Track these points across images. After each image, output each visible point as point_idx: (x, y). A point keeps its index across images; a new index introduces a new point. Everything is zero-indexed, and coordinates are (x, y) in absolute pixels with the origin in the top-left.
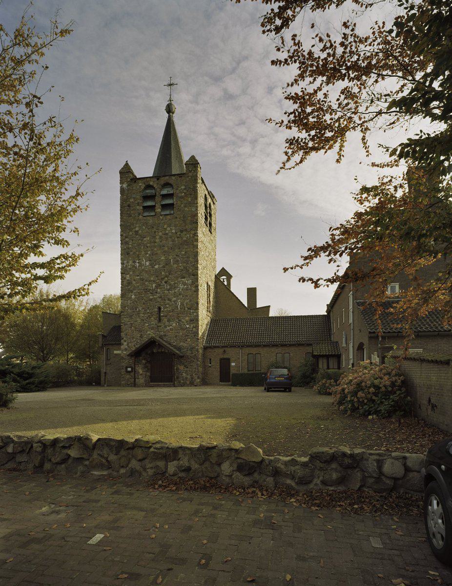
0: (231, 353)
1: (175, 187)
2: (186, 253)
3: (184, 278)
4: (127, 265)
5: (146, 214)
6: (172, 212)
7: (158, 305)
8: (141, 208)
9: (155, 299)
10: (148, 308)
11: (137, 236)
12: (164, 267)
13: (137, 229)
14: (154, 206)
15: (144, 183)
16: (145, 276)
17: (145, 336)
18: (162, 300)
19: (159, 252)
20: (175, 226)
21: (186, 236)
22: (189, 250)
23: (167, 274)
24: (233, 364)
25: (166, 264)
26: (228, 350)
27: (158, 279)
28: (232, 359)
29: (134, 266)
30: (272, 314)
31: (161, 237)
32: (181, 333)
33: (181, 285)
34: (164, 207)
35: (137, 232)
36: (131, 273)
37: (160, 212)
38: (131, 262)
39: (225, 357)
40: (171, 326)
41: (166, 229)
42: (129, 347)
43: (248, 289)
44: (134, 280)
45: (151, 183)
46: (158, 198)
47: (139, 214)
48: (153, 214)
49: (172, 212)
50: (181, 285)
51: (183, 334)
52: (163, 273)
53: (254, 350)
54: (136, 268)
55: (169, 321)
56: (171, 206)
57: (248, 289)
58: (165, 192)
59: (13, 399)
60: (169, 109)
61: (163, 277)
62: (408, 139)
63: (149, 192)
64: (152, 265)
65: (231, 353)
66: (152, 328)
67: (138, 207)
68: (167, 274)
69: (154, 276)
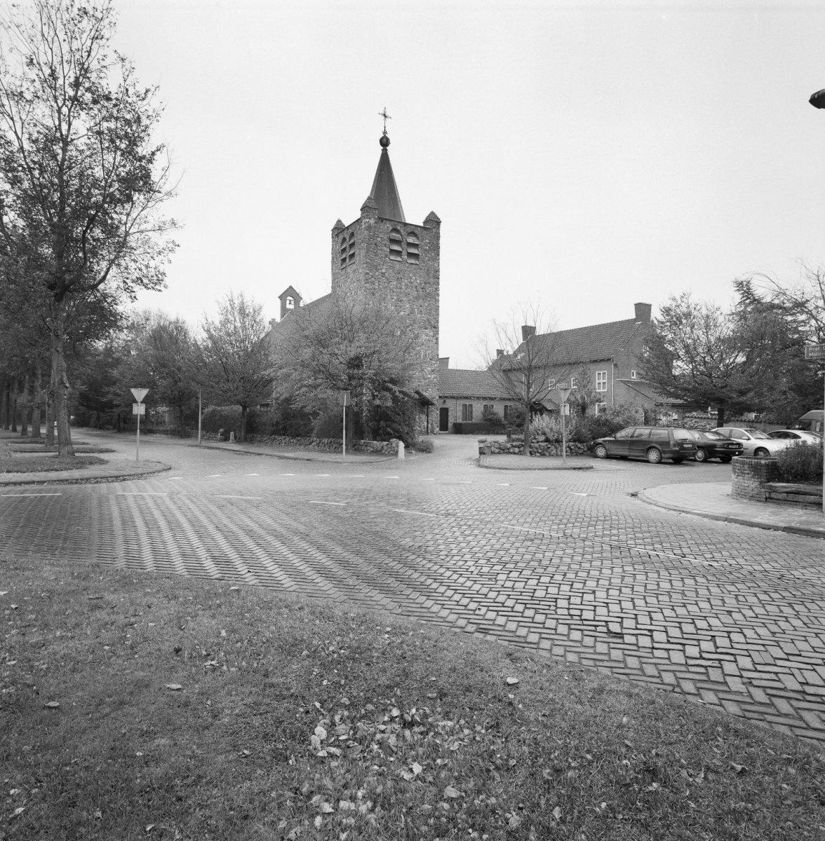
13: (384, 271)
14: (401, 252)
19: (404, 299)
20: (420, 277)
26: (448, 401)
30: (451, 366)
31: (406, 285)
34: (410, 255)
35: (384, 273)
41: (411, 278)
43: (291, 287)
45: (416, 232)
47: (386, 256)
53: (467, 402)
56: (415, 256)
57: (291, 287)
59: (156, 358)
60: (385, 142)
63: (395, 236)
65: (450, 404)
67: (385, 248)
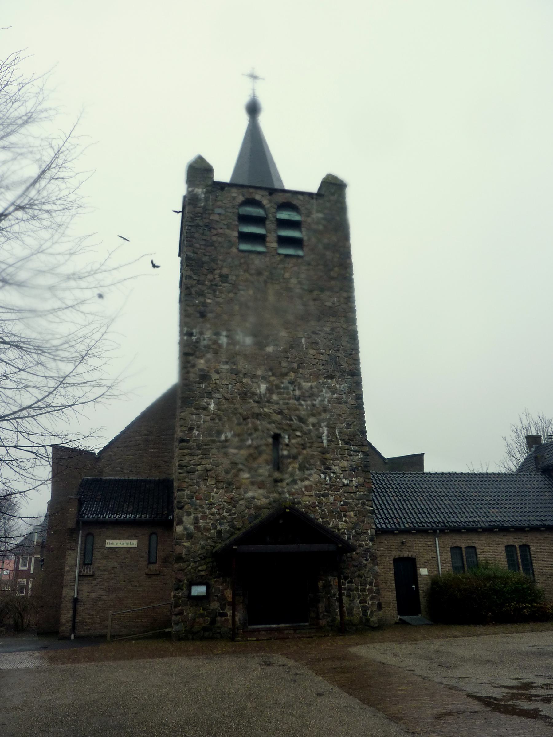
0: (416, 547)
1: (304, 212)
2: (332, 329)
3: (332, 378)
4: (199, 338)
5: (244, 247)
6: (300, 253)
7: (273, 429)
8: (236, 234)
9: (266, 415)
10: (250, 434)
11: (225, 285)
12: (286, 351)
15: (243, 195)
16: (244, 365)
17: (242, 502)
18: (285, 417)
21: (331, 300)
22: (337, 325)
23: (295, 366)
24: (424, 571)
25: (292, 347)
27: (273, 375)
28: (420, 560)
29: (215, 342)
30: (429, 467)
32: (331, 498)
33: (327, 393)
34: (284, 241)
36: (209, 356)
37: (276, 249)
38: (208, 334)
39: (406, 554)
40: (308, 479)
42: (198, 528)
44: (217, 372)
45: (258, 197)
46: (271, 225)
48: (261, 249)
49: (300, 253)
50: (327, 393)
51: (335, 500)
52: (284, 364)
54: (220, 346)
55: (302, 468)
58: (284, 215)
61: (284, 370)
62: (333, 188)
64: (260, 345)
66: (261, 485)
68: (295, 366)
69: (263, 367)
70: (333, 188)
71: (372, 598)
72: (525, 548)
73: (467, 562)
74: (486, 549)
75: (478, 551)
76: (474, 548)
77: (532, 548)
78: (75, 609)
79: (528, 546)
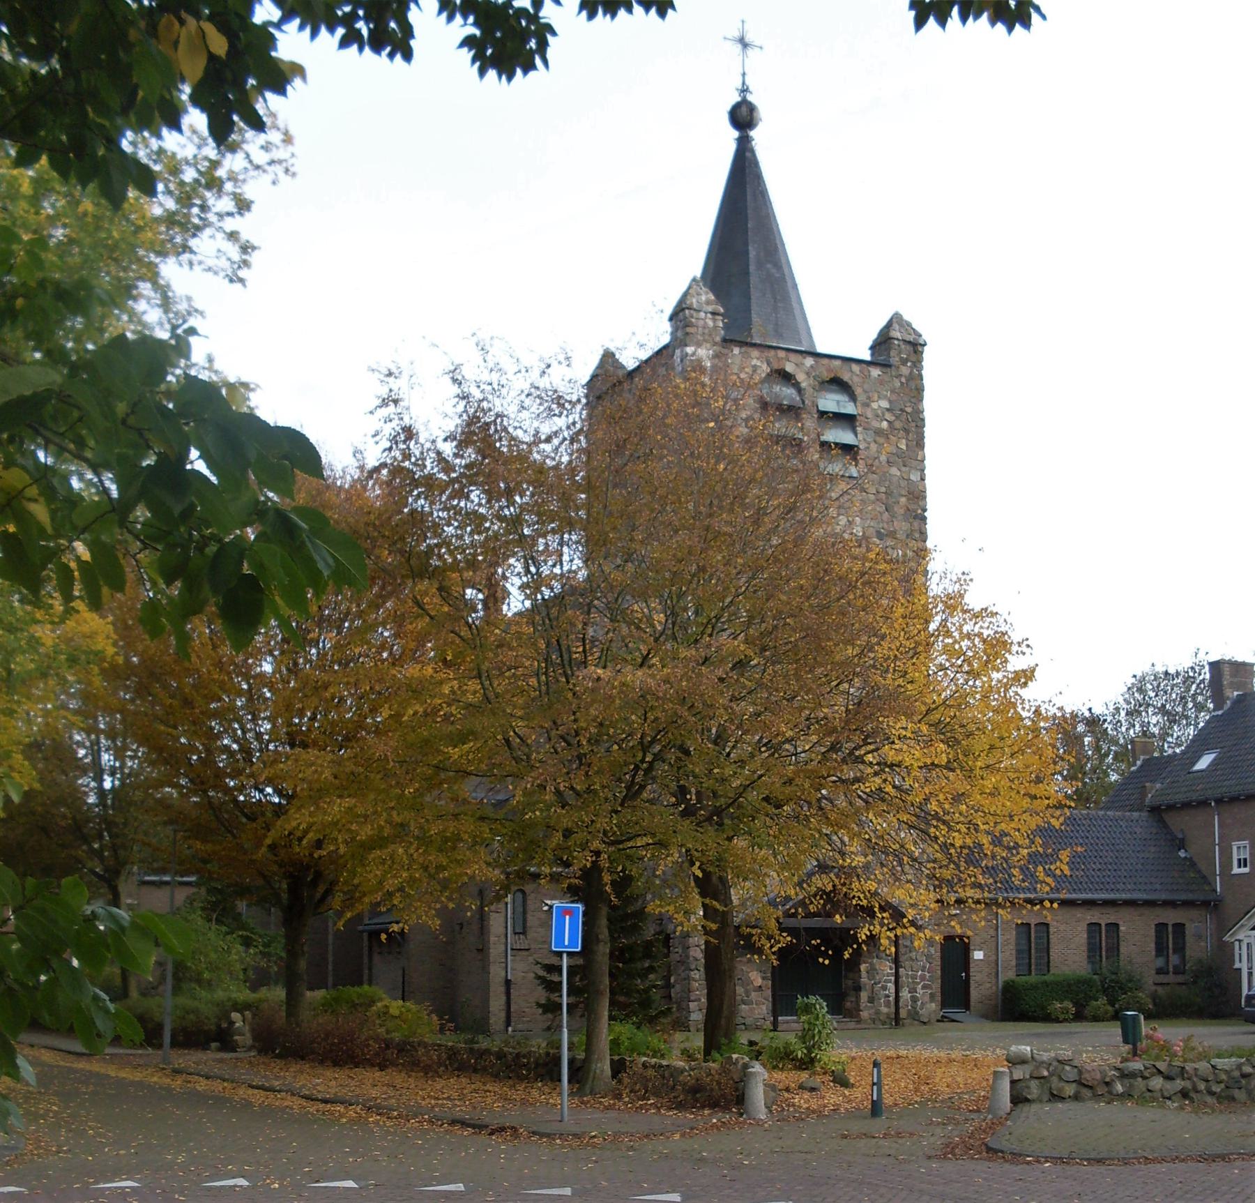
15: (769, 364)
70: (898, 349)
71: (924, 987)
72: (1113, 927)
73: (1036, 944)
74: (1062, 928)
75: (1052, 930)
76: (1047, 925)
77: (1122, 928)
78: (508, 994)
79: (1117, 925)
